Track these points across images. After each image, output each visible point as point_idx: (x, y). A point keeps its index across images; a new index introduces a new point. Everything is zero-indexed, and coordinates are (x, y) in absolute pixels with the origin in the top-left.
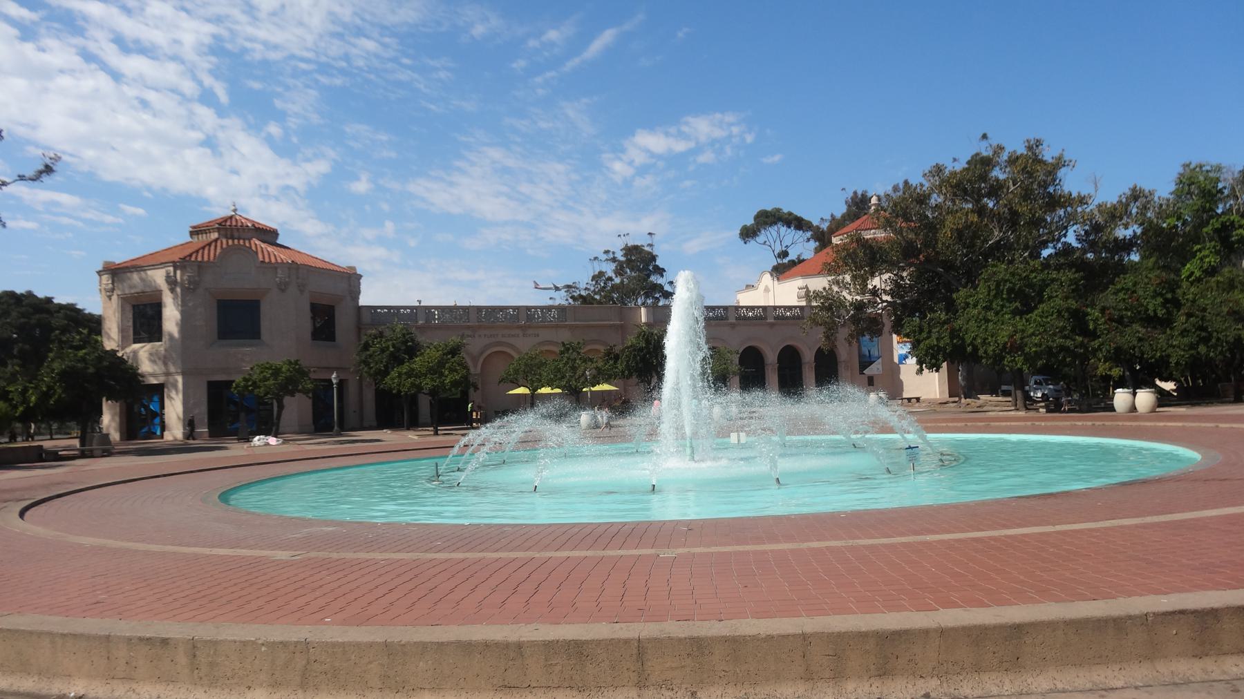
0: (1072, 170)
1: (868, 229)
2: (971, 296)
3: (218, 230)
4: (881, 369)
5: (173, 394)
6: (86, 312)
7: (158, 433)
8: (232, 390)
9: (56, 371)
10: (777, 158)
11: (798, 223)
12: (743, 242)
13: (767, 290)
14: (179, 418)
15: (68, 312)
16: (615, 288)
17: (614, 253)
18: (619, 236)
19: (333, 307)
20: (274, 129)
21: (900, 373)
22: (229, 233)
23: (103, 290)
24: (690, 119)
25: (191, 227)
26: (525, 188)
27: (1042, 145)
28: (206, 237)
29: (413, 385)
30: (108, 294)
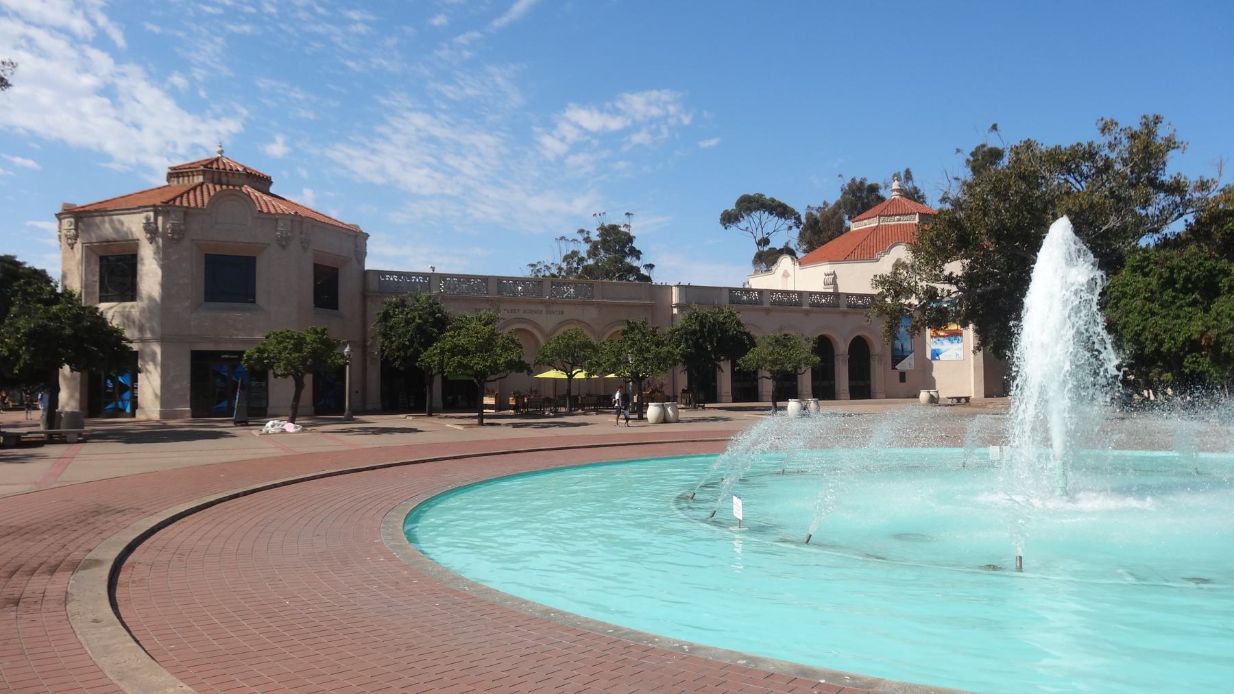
0: (1183, 153)
1: (893, 215)
2: (1127, 285)
3: (204, 173)
4: (913, 364)
5: (150, 367)
6: (27, 266)
7: (128, 410)
8: (242, 362)
9: (23, 331)
10: (713, 142)
11: (781, 211)
12: (723, 228)
13: (786, 275)
14: (156, 395)
15: (6, 265)
16: (588, 271)
17: (588, 233)
18: (595, 215)
19: (337, 269)
20: (178, 80)
21: (932, 370)
22: (216, 177)
23: (63, 237)
24: (627, 96)
25: (169, 168)
26: (452, 161)
27: (1161, 122)
28: (189, 180)
29: (460, 364)
30: (70, 241)
